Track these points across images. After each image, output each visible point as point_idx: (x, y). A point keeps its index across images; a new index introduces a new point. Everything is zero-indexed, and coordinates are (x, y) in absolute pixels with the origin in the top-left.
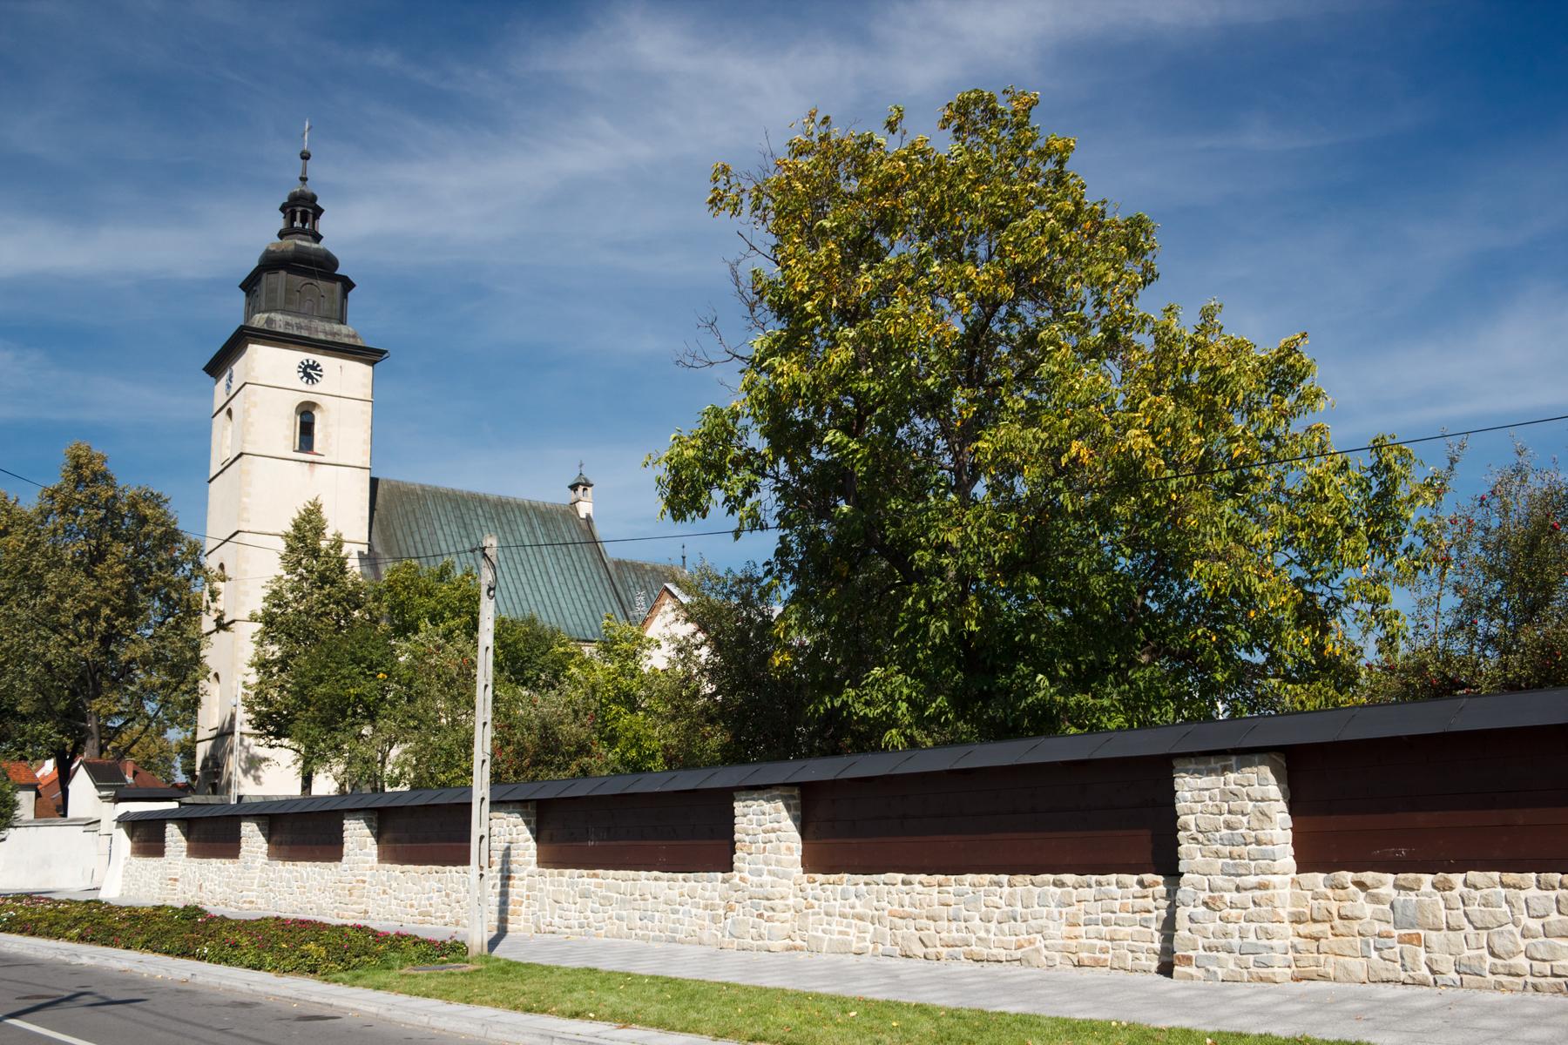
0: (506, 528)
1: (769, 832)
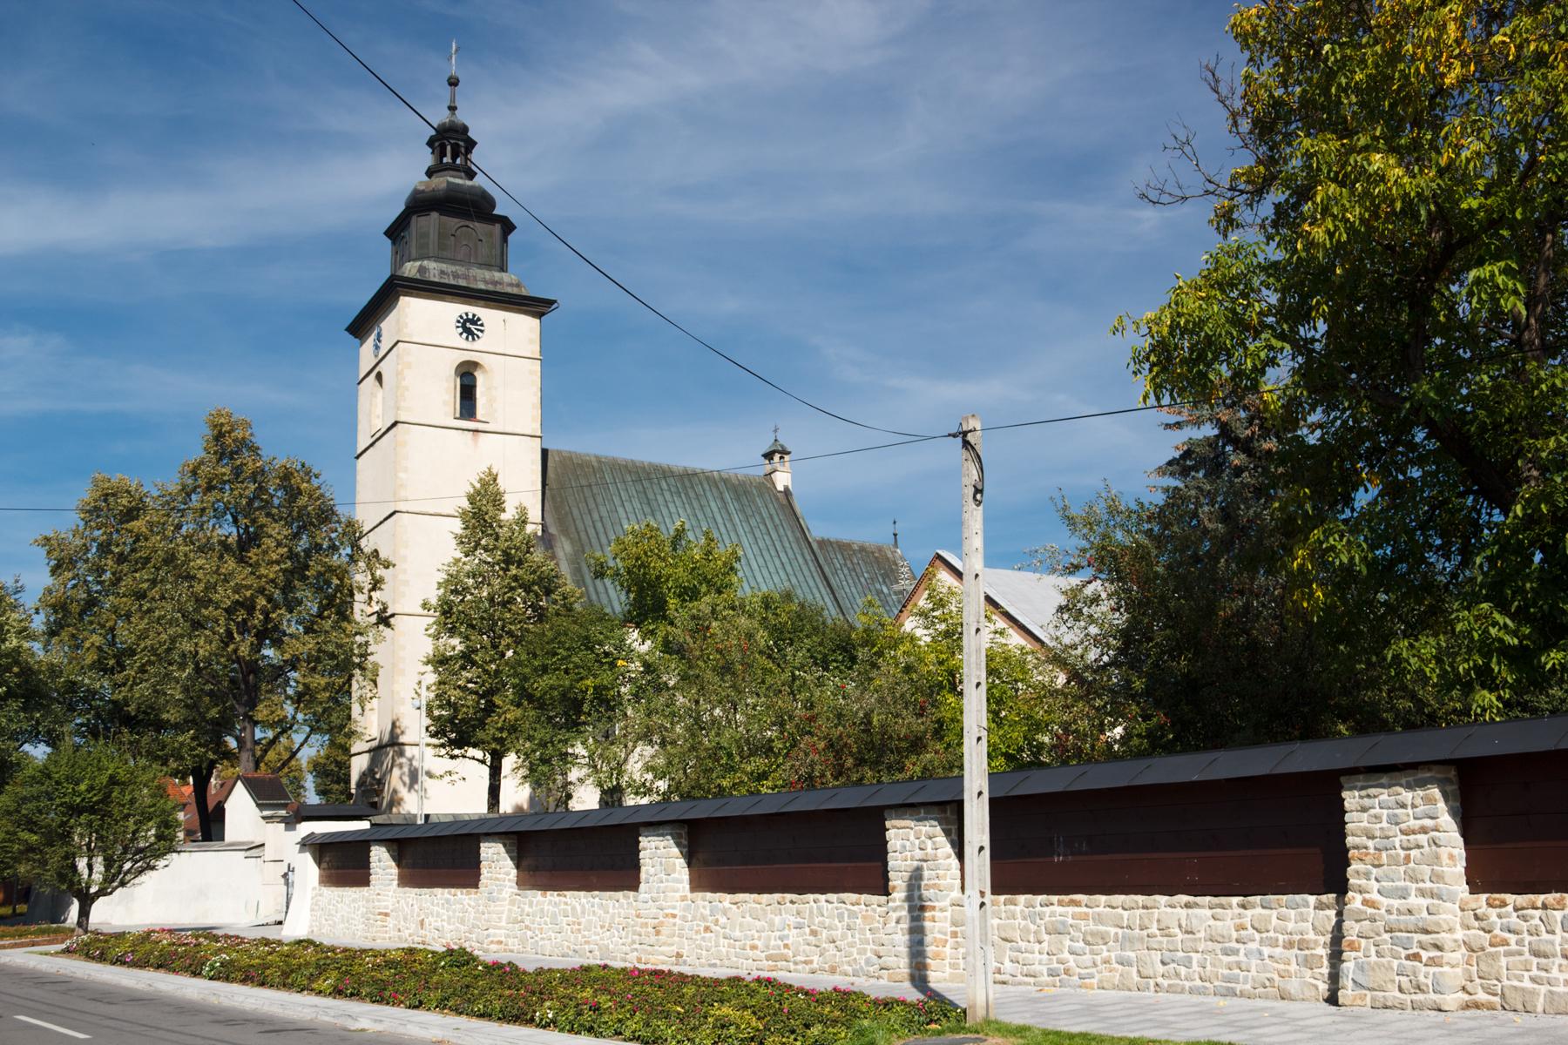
1: (1414, 833)
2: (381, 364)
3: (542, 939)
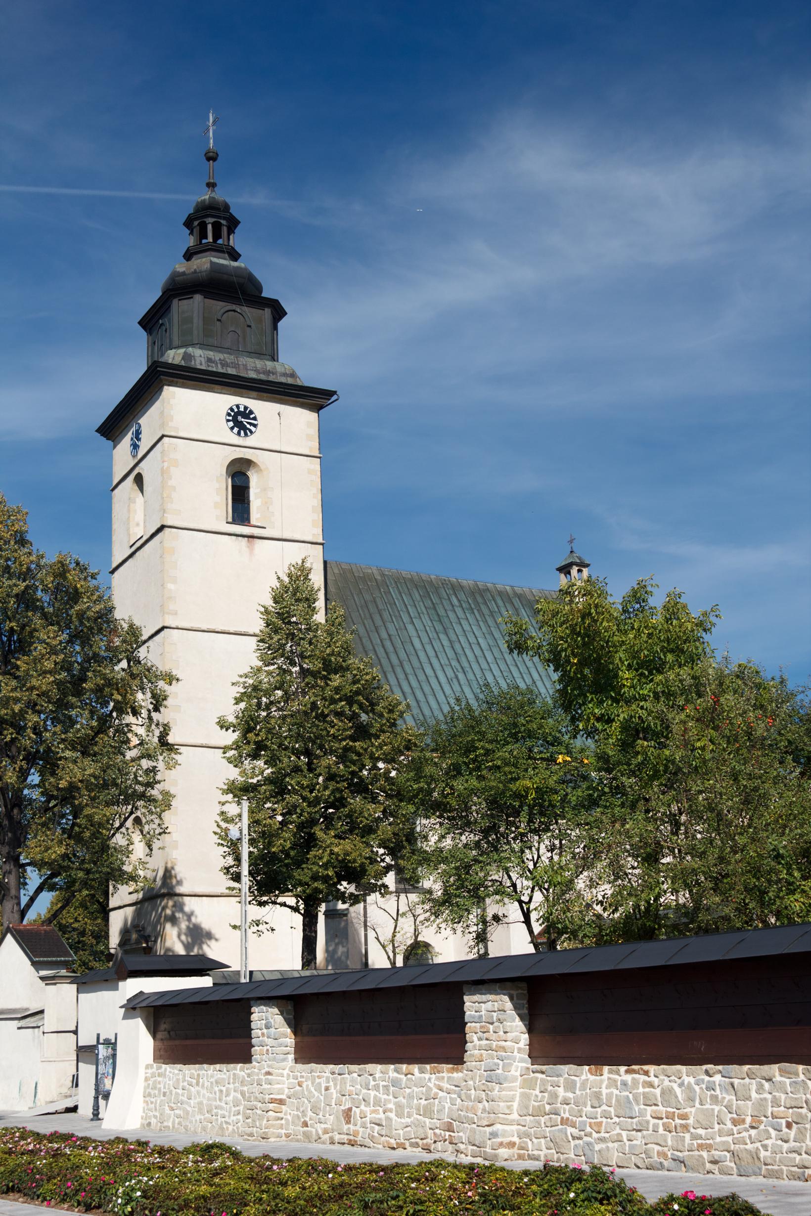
0: (490, 622)
2: (141, 465)
3: (602, 1140)
